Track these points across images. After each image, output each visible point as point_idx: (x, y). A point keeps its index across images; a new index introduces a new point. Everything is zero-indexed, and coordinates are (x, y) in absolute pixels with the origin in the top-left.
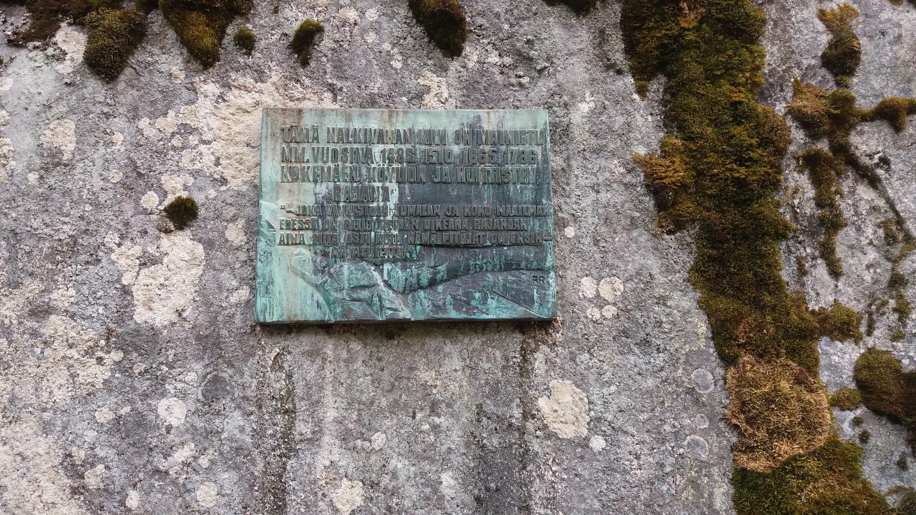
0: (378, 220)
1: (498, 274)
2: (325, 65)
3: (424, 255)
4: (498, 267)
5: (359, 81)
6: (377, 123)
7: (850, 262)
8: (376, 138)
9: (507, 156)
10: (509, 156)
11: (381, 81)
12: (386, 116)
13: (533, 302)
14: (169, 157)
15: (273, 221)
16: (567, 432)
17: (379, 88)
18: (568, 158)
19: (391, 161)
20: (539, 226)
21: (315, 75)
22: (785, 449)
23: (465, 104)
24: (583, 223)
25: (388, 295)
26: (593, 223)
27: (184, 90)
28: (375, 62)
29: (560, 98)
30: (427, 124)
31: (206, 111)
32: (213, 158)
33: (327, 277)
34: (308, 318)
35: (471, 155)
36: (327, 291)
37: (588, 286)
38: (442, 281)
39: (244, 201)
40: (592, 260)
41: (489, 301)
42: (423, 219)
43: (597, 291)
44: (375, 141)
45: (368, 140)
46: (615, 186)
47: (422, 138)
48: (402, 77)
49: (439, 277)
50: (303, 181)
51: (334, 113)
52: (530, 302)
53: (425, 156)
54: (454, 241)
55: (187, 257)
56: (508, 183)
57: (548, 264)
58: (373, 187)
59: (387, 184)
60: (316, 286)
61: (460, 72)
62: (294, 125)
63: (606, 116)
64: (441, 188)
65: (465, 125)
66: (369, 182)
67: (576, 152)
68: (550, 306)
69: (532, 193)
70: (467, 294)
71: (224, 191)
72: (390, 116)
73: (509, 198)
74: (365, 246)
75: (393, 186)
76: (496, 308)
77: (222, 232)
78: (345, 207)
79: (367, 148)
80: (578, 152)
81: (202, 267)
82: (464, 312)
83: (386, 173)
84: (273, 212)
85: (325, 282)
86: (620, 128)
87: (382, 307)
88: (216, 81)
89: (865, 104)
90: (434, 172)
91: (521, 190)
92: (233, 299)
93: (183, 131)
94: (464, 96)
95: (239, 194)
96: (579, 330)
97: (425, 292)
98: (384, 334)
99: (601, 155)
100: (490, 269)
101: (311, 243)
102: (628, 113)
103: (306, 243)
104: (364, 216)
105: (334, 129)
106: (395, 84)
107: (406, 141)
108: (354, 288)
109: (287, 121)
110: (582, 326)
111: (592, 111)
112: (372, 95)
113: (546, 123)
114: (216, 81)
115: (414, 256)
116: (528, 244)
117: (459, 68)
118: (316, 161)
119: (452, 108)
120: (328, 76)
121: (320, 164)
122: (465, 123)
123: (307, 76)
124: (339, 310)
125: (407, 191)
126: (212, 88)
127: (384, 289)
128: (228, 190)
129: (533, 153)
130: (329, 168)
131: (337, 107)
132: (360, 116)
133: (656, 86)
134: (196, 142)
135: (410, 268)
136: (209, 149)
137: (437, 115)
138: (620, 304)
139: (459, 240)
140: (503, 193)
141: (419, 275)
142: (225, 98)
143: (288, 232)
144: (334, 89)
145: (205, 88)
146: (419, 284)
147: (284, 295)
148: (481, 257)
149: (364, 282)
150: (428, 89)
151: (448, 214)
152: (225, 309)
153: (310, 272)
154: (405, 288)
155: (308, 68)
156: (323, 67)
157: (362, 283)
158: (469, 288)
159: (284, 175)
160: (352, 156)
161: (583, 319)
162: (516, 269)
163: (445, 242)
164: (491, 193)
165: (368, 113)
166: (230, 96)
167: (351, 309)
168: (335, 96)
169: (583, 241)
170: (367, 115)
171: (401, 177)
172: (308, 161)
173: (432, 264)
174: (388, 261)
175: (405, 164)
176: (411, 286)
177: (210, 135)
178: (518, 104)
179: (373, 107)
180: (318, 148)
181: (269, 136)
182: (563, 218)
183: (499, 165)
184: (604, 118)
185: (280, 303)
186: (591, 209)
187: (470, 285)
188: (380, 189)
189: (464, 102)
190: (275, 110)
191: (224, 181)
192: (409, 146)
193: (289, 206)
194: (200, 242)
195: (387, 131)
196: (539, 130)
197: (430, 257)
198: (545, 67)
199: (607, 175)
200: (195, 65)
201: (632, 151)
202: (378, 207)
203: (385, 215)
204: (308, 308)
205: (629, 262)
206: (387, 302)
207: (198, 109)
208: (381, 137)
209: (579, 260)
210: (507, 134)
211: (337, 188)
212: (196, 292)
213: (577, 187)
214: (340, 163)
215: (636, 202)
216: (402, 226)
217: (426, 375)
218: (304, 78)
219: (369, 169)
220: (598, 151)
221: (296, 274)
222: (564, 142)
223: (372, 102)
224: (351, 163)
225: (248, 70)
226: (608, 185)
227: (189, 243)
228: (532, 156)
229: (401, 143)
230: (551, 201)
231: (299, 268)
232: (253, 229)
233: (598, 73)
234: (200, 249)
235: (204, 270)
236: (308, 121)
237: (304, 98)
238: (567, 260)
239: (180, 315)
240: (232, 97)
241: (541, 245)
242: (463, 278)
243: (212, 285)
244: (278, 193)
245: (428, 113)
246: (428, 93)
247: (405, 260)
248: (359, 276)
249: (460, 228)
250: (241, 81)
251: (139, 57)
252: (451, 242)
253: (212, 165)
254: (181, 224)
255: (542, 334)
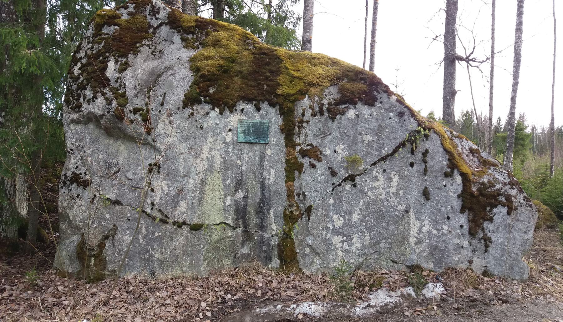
7: (301, 138)
16: (269, 154)
22: (290, 157)
37: (273, 139)
89: (305, 120)
126: (232, 115)
133: (282, 116)
208: (251, 123)
217: (255, 148)
232: (237, 131)
236: (243, 121)
251: (225, 112)
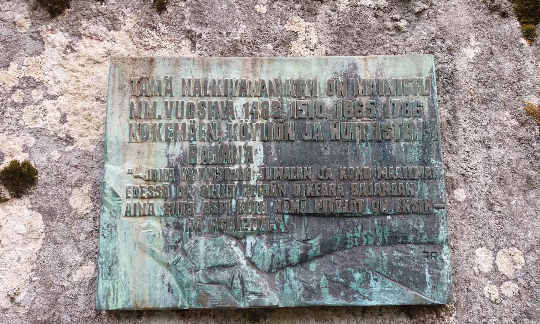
0: (240, 186)
1: (381, 249)
2: (183, 10)
3: (293, 226)
4: (381, 240)
5: (221, 27)
6: (238, 73)
8: (238, 90)
9: (388, 109)
10: (391, 109)
11: (244, 26)
12: (249, 65)
13: (424, 284)
14: (7, 115)
15: (119, 188)
17: (242, 35)
18: (454, 109)
19: (254, 116)
20: (429, 191)
21: (172, 21)
23: (336, 51)
24: (474, 184)
25: (252, 276)
26: (486, 184)
27: (29, 39)
28: (238, 7)
29: (443, 42)
30: (295, 74)
31: (53, 63)
32: (58, 114)
33: (180, 255)
34: (157, 305)
35: (346, 109)
36: (179, 272)
38: (315, 257)
39: (91, 163)
40: (487, 227)
41: (372, 283)
42: (291, 183)
43: (494, 264)
44: (237, 94)
45: (229, 92)
46: (508, 140)
47: (290, 89)
48: (268, 22)
49: (311, 252)
50: (154, 140)
51: (190, 62)
52: (421, 284)
53: (293, 110)
54: (328, 209)
55: (23, 230)
56: (390, 140)
57: (441, 237)
58: (235, 147)
59: (251, 143)
60: (168, 265)
61: (330, 16)
62: (145, 76)
63: (493, 62)
64: (312, 146)
65: (339, 74)
66: (230, 141)
67: (463, 102)
68: (445, 288)
69: (419, 151)
70: (345, 275)
71: (69, 152)
72: (254, 65)
73: (392, 158)
74: (224, 217)
75: (257, 145)
76: (381, 291)
77: (66, 199)
78: (202, 171)
79: (227, 102)
80: (466, 102)
81: (41, 241)
82: (342, 297)
83: (249, 130)
84: (119, 177)
85: (178, 261)
86: (510, 76)
87: (244, 291)
88: (65, 30)
90: (304, 128)
91: (406, 148)
92: (76, 278)
93: (25, 85)
94: (334, 41)
95: (86, 154)
96: (476, 313)
97: (295, 271)
98: (248, 315)
99: (490, 106)
100: (371, 242)
101: (162, 214)
102: (517, 59)
103: (156, 213)
104: (224, 180)
105: (189, 81)
106: (260, 30)
107: (272, 93)
108: (211, 269)
109: (137, 72)
110: (479, 308)
111: (479, 57)
112: (234, 43)
113: (432, 70)
114: (65, 30)
115: (282, 227)
116: (416, 213)
117: (329, 12)
118: (169, 117)
119: (322, 56)
120: (186, 22)
121: (174, 120)
122: (339, 72)
123: (163, 23)
124: (193, 294)
125: (273, 151)
127: (247, 268)
128: (74, 150)
129: (418, 105)
130: (184, 125)
131: (196, 55)
132: (220, 65)
134: (40, 97)
135: (277, 242)
136: (55, 104)
137: (307, 63)
138: (522, 281)
139: (334, 209)
140: (384, 152)
141: (287, 250)
142: (75, 48)
143: (136, 201)
144: (192, 36)
145: (52, 38)
146: (287, 261)
147: (130, 276)
148: (360, 228)
149: (223, 261)
150: (295, 35)
151: (321, 177)
152: (66, 289)
153: (160, 249)
154: (271, 266)
155: (165, 14)
156: (181, 12)
157: (220, 262)
158: (347, 266)
159: (132, 135)
160: (210, 111)
161: (479, 299)
162: (402, 243)
163: (317, 211)
164: (370, 152)
165: (229, 61)
166: (80, 46)
167: (208, 295)
168: (194, 43)
169: (475, 205)
170: (227, 64)
171: (266, 134)
172: (160, 118)
173: (303, 237)
174: (252, 233)
175: (271, 120)
176: (278, 264)
177: (56, 89)
178: (395, 49)
179: (235, 55)
180: (172, 103)
181: (116, 90)
182: (452, 179)
183: (378, 120)
184: (492, 64)
185: (125, 286)
186: (482, 167)
187: (349, 263)
188: (243, 149)
189: (334, 48)
190: (124, 60)
191: (69, 140)
192: (275, 99)
193: (138, 170)
194: (39, 211)
195: (250, 82)
196: (424, 78)
197: (300, 228)
198: (425, 10)
199: (499, 128)
200: (42, 13)
201: (524, 102)
202: (240, 170)
203: (248, 179)
204: (157, 293)
205: (528, 229)
206: (250, 285)
207: (44, 60)
209: (472, 228)
210: (388, 84)
211: (193, 149)
212: (33, 270)
213: (466, 142)
214: (196, 119)
215: (532, 159)
216: (268, 192)
218: (160, 24)
219: (229, 126)
220: (487, 101)
221: (144, 251)
222: (448, 91)
223: (235, 50)
224: (210, 119)
225: (101, 17)
226: (500, 140)
227: (27, 213)
228: (418, 108)
229: (266, 96)
230: (441, 161)
231: (148, 245)
233: (481, 16)
234: (38, 220)
235: (43, 245)
237: (160, 47)
238: (458, 227)
239: (13, 299)
240: (82, 47)
241: (432, 213)
242: (340, 254)
243: (52, 263)
244: (125, 155)
245: (297, 61)
246: (296, 39)
247: (272, 232)
248: (217, 254)
249: (335, 194)
250: (93, 29)
252: (325, 210)
253: (56, 122)
254: (17, 192)
255: (432, 318)
